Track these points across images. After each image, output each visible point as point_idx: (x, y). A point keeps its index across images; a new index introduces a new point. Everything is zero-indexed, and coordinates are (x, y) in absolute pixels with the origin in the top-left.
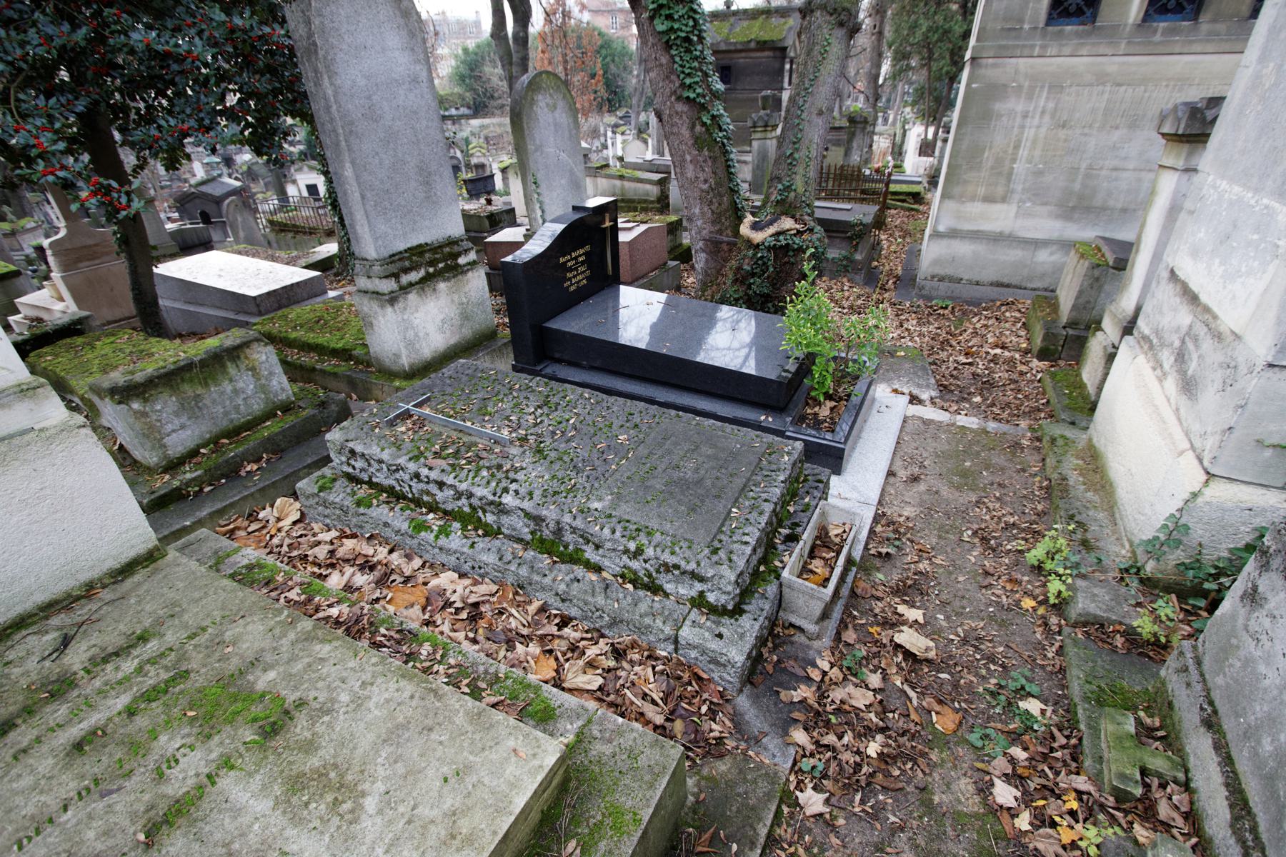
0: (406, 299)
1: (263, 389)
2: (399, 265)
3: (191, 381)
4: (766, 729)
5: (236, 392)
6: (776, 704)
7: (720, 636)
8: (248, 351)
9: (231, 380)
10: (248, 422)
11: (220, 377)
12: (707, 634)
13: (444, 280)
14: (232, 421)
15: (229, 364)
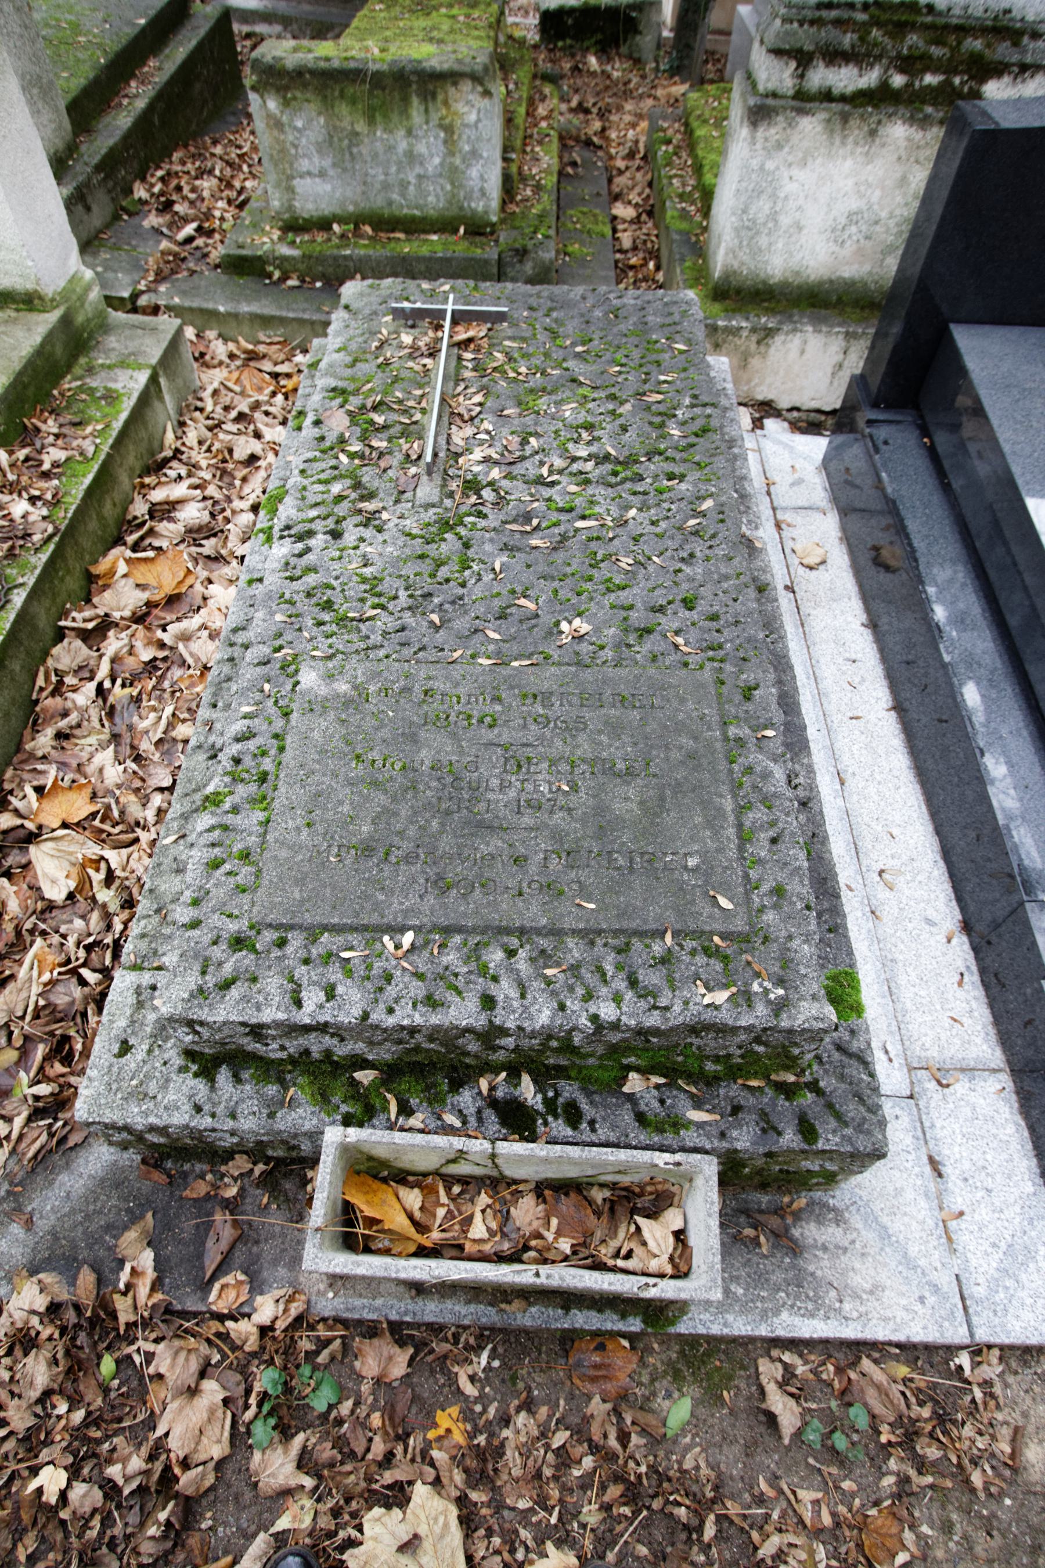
0: (791, 124)
1: (453, 174)
2: (827, 34)
3: (353, 102)
4: (43, 1225)
5: (411, 157)
6: (109, 1228)
7: (125, 1048)
8: (452, 91)
9: (409, 132)
10: (413, 219)
11: (395, 117)
12: (123, 1023)
13: (911, 120)
14: (390, 203)
15: (415, 101)
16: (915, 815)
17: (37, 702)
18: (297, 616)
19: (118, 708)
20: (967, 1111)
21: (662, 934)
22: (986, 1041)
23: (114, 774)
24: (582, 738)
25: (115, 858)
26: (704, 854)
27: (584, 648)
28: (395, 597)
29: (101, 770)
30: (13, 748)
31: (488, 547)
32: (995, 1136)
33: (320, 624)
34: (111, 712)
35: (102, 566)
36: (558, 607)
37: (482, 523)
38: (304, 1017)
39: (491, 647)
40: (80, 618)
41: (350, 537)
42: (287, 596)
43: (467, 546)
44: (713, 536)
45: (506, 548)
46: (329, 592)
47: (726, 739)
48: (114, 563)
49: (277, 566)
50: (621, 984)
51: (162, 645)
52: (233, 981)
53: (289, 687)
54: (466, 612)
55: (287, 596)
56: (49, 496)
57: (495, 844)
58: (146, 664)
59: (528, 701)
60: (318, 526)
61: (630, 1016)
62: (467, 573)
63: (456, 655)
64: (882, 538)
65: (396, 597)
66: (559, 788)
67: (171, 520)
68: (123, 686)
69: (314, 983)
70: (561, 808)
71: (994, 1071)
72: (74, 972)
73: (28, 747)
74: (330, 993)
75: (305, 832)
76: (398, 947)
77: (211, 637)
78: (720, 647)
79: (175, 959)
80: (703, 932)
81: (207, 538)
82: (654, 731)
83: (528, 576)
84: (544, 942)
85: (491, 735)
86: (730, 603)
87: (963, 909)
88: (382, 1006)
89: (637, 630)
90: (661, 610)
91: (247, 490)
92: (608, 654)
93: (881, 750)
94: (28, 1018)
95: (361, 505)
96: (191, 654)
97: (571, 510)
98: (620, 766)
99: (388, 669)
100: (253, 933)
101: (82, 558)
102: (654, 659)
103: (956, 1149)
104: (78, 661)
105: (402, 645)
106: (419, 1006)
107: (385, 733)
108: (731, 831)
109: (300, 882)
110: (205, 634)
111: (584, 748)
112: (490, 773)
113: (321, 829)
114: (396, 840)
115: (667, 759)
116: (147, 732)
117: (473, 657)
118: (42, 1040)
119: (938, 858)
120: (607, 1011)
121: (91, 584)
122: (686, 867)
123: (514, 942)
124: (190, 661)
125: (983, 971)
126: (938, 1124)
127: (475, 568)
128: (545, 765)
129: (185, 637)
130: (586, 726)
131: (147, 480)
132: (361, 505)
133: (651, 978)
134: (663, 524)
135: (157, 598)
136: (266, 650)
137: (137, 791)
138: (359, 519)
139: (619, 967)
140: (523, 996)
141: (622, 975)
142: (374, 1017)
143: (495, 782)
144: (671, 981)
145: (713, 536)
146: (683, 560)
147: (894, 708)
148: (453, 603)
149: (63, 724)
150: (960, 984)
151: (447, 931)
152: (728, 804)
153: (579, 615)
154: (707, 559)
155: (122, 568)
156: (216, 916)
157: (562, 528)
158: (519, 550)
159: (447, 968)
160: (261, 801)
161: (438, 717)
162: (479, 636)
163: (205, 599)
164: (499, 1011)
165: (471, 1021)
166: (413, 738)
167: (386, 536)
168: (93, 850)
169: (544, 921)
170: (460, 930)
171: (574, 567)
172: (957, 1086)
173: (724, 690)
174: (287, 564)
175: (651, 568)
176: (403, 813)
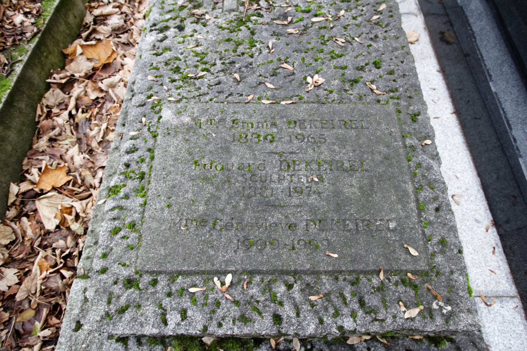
7: (79, 326)
12: (76, 311)
16: (467, 167)
17: (38, 122)
18: (161, 76)
19: (80, 124)
20: (500, 318)
21: (378, 273)
22: (507, 282)
23: (79, 159)
24: (323, 148)
25: (78, 206)
26: (398, 219)
27: (321, 92)
28: (214, 64)
29: (72, 158)
30: (27, 147)
31: (264, 34)
32: (514, 331)
33: (173, 81)
34: (77, 127)
35: (69, 50)
36: (305, 68)
37: (261, 20)
38: (169, 331)
39: (269, 93)
40: (58, 78)
41: (188, 30)
42: (154, 65)
43: (253, 33)
44: (387, 25)
45: (274, 34)
46: (178, 62)
47: (405, 146)
48: (76, 47)
49: (149, 47)
50: (356, 306)
51: (101, 91)
52: (127, 307)
53: (156, 120)
54: (254, 72)
55: (154, 65)
56: (34, 12)
57: (276, 217)
58: (93, 100)
59: (292, 126)
60: (171, 23)
61: (362, 326)
62: (254, 49)
63: (250, 98)
64: (444, 28)
65: (214, 64)
66: (312, 180)
67: (105, 24)
68: (83, 112)
69: (174, 309)
70: (314, 192)
71: (512, 297)
72: (58, 271)
73: (34, 147)
74: (184, 314)
75: (166, 211)
76: (223, 284)
77: (125, 86)
78: (397, 90)
79: (92, 294)
80: (401, 271)
81: (123, 33)
82: (364, 142)
83: (287, 51)
84: (308, 279)
85: (272, 147)
86: (400, 64)
87: (493, 215)
88: (215, 322)
89: (350, 81)
90: (362, 69)
91: (142, 8)
92: (335, 96)
93: (449, 134)
94: (38, 294)
95: (194, 11)
96: (116, 95)
97: (308, 12)
98: (347, 165)
99: (211, 107)
100: (137, 276)
101: (58, 45)
102: (360, 98)
103: (496, 338)
104: (59, 100)
105: (219, 92)
106: (237, 322)
107: (211, 147)
108: (413, 205)
109: (164, 243)
110: (122, 84)
111: (326, 155)
112: (272, 171)
113: (176, 209)
114: (219, 215)
115: (373, 160)
116: (95, 137)
117: (259, 99)
118: (45, 306)
119: (480, 188)
120: (348, 324)
121: (65, 59)
122: (388, 229)
123: (291, 279)
124: (115, 98)
125: (504, 247)
126: (487, 325)
127: (258, 46)
128: (303, 165)
129: (113, 86)
130: (326, 140)
131: (93, 4)
132: (194, 11)
133: (373, 301)
134: (360, 19)
135: (98, 65)
136: (143, 97)
137: (90, 169)
138: (193, 19)
139: (353, 294)
140: (298, 315)
141: (356, 299)
142: (210, 329)
143: (275, 177)
144: (384, 301)
145: (387, 25)
146: (371, 39)
147: (454, 113)
148: (246, 67)
149: (52, 134)
150: (494, 252)
151: (252, 273)
152: (410, 188)
153: (317, 73)
154: (385, 38)
155: (79, 50)
156: (116, 266)
157: (305, 22)
158: (281, 35)
159: (252, 297)
160: (141, 191)
161: (241, 137)
162: (262, 87)
163: (122, 65)
164: (284, 325)
165: (268, 331)
166: (227, 150)
167: (208, 28)
168: (68, 202)
169: (308, 266)
170: (259, 272)
171: (313, 44)
172: (495, 306)
173: (402, 116)
174: (154, 46)
175: (355, 44)
176: (223, 198)
